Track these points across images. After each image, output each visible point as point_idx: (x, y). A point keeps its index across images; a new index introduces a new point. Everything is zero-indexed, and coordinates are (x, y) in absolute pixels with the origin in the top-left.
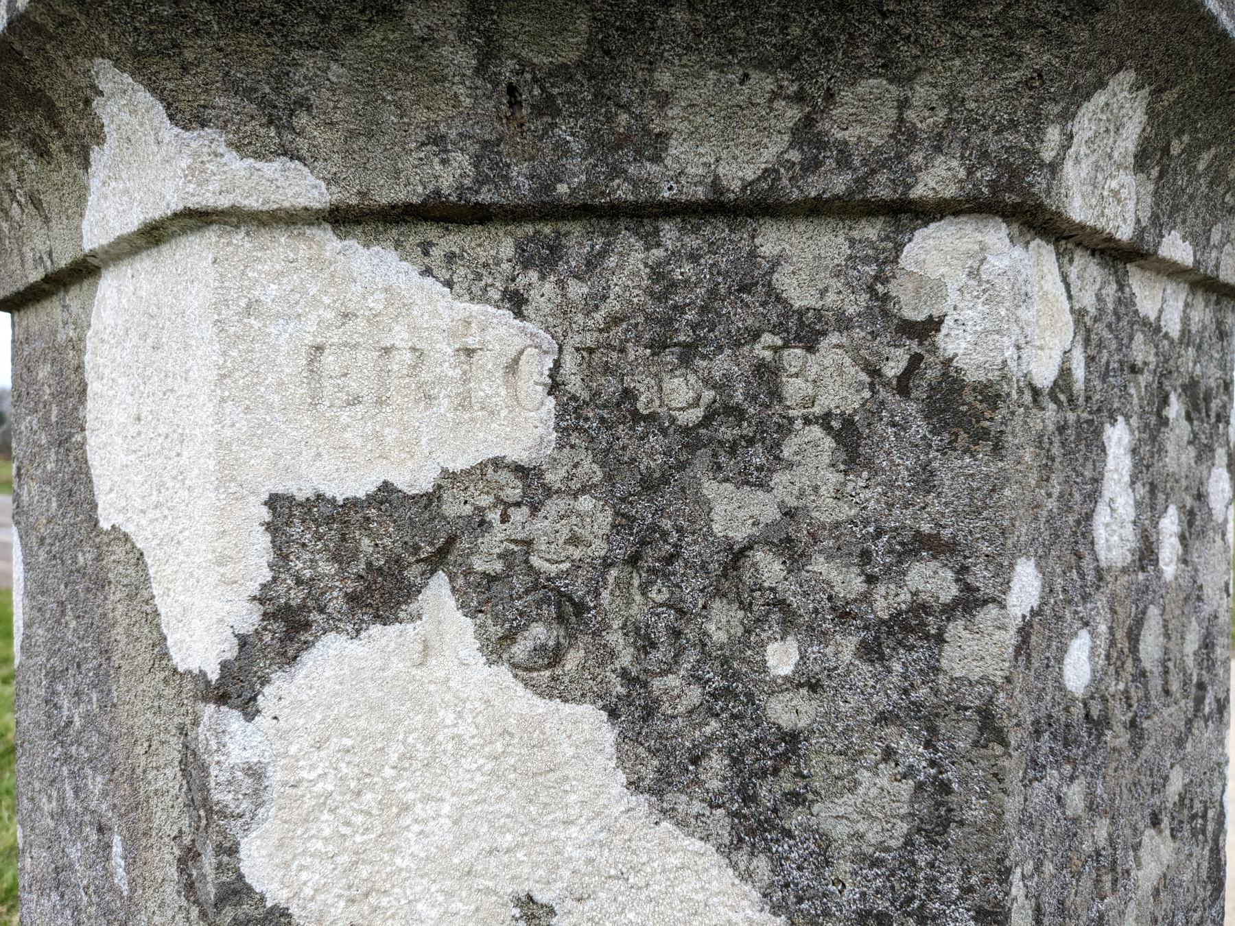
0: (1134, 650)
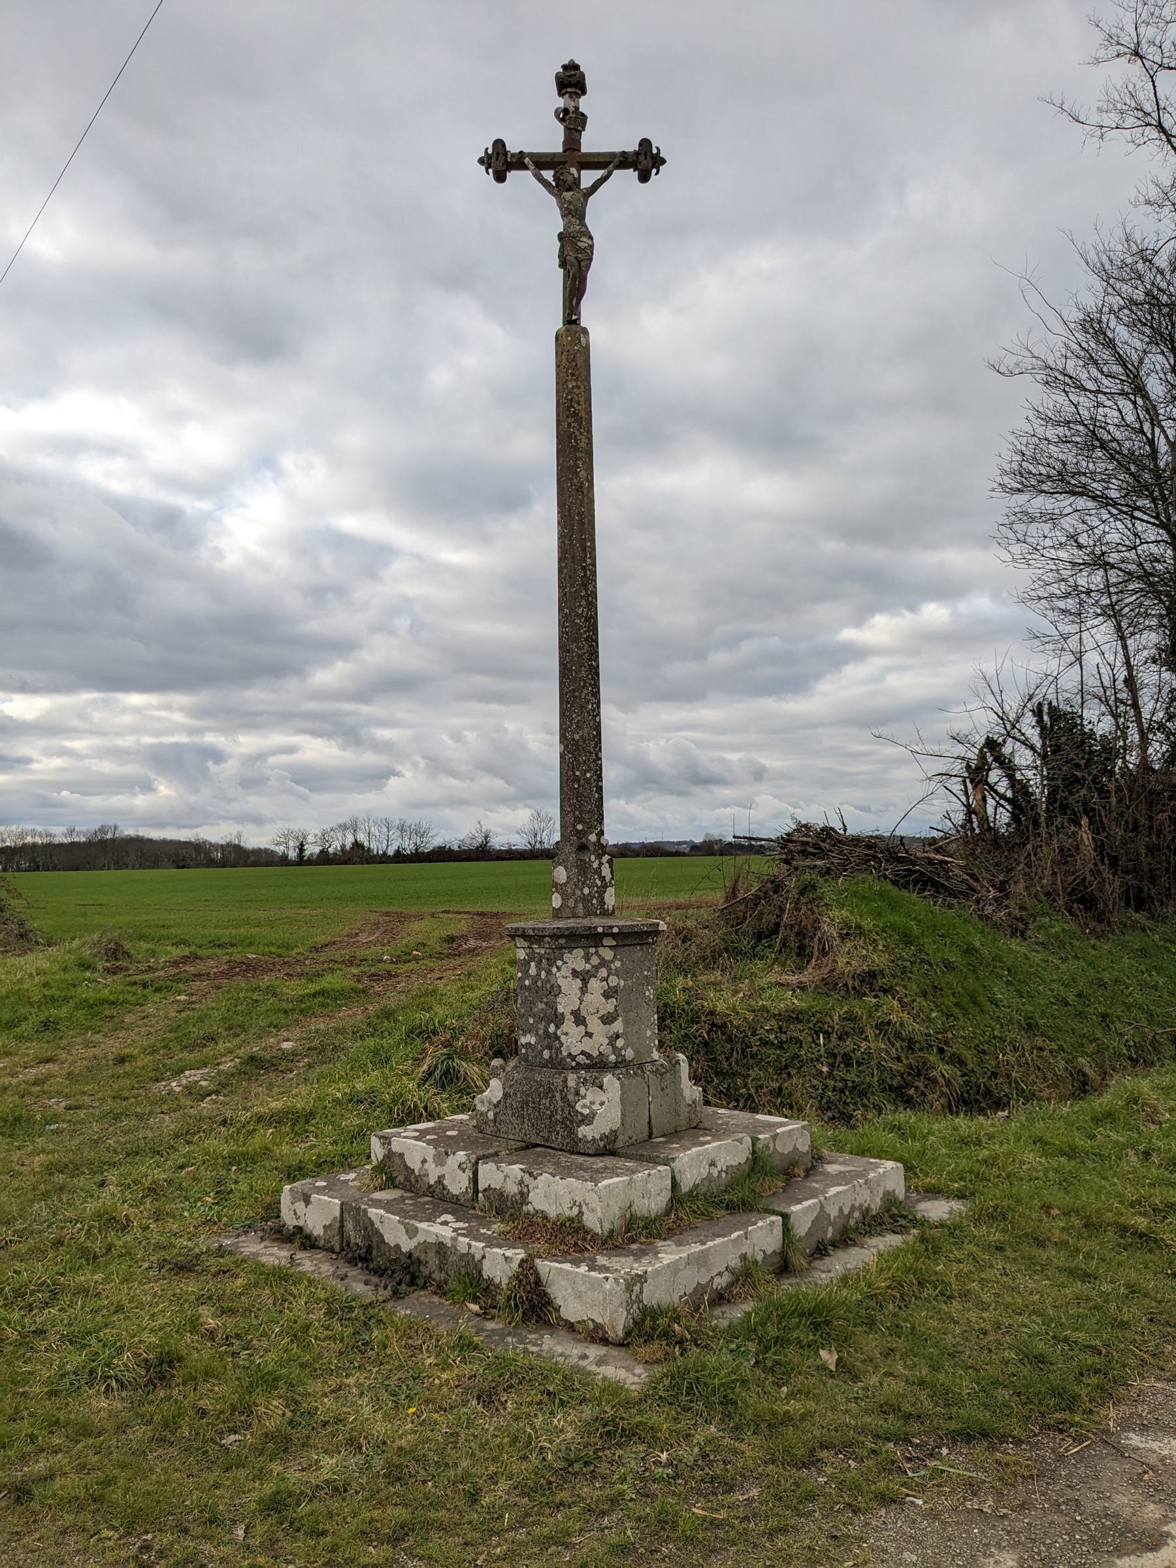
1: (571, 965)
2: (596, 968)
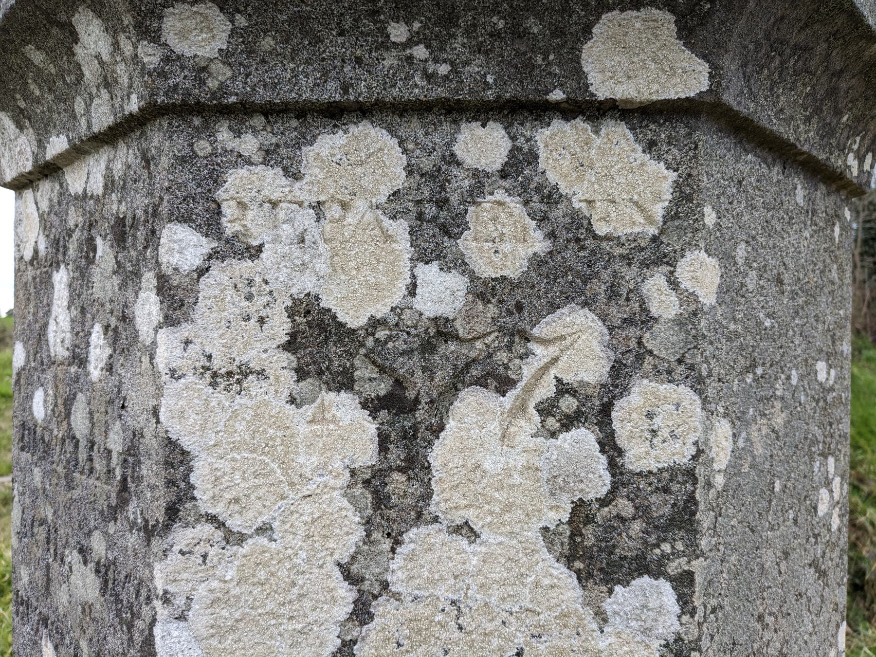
0: (68, 415)
1: (287, 271)
2: (514, 306)
